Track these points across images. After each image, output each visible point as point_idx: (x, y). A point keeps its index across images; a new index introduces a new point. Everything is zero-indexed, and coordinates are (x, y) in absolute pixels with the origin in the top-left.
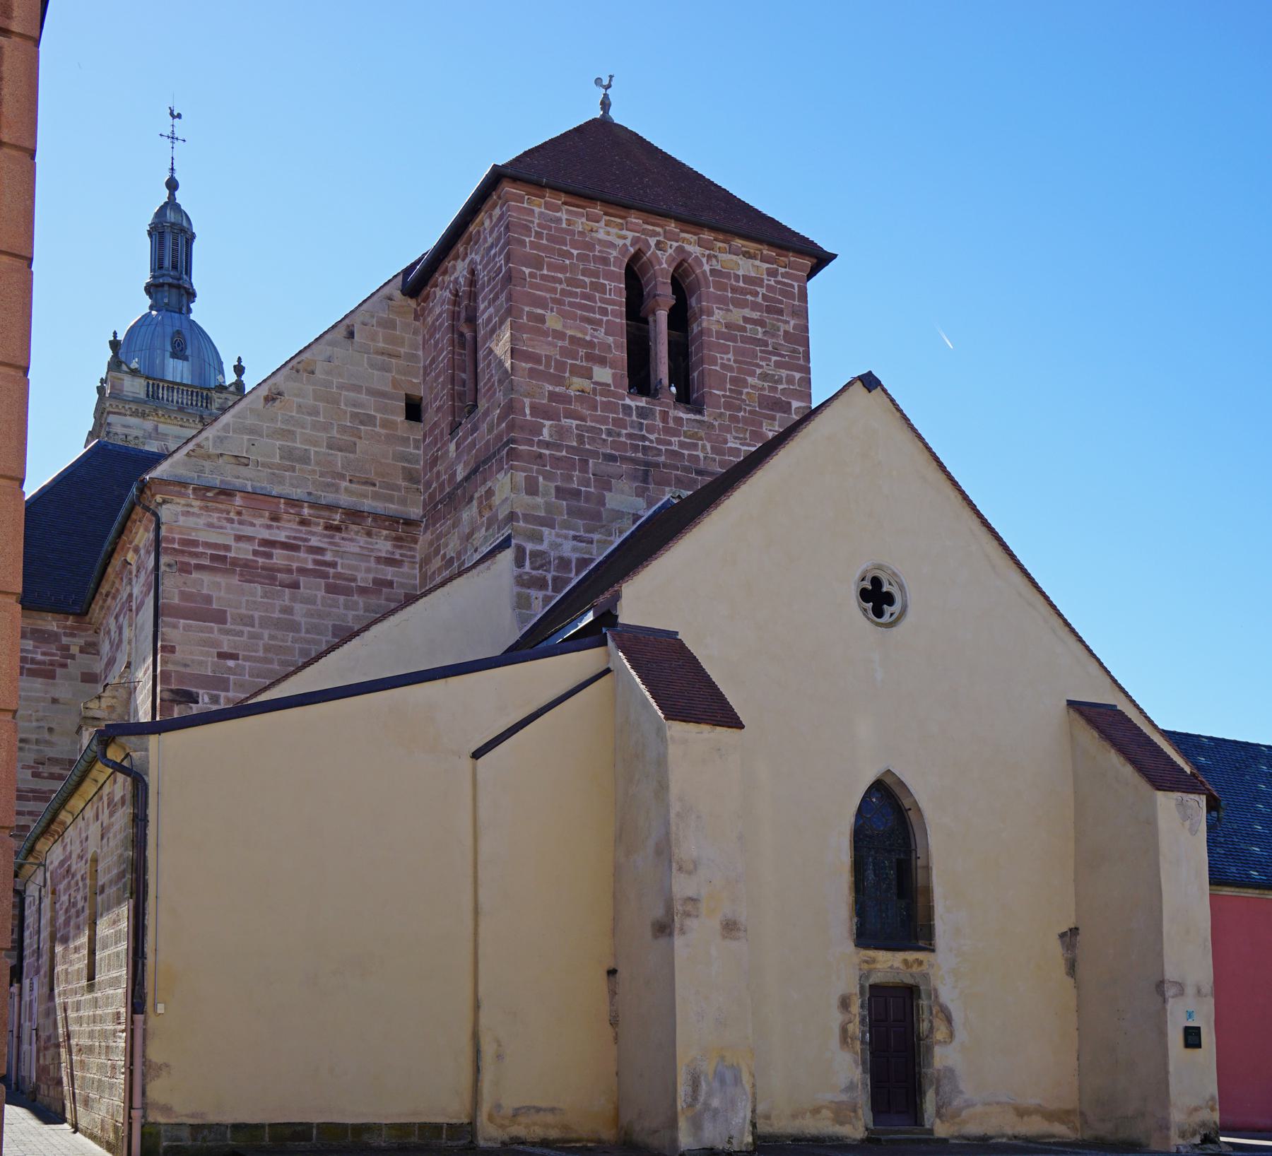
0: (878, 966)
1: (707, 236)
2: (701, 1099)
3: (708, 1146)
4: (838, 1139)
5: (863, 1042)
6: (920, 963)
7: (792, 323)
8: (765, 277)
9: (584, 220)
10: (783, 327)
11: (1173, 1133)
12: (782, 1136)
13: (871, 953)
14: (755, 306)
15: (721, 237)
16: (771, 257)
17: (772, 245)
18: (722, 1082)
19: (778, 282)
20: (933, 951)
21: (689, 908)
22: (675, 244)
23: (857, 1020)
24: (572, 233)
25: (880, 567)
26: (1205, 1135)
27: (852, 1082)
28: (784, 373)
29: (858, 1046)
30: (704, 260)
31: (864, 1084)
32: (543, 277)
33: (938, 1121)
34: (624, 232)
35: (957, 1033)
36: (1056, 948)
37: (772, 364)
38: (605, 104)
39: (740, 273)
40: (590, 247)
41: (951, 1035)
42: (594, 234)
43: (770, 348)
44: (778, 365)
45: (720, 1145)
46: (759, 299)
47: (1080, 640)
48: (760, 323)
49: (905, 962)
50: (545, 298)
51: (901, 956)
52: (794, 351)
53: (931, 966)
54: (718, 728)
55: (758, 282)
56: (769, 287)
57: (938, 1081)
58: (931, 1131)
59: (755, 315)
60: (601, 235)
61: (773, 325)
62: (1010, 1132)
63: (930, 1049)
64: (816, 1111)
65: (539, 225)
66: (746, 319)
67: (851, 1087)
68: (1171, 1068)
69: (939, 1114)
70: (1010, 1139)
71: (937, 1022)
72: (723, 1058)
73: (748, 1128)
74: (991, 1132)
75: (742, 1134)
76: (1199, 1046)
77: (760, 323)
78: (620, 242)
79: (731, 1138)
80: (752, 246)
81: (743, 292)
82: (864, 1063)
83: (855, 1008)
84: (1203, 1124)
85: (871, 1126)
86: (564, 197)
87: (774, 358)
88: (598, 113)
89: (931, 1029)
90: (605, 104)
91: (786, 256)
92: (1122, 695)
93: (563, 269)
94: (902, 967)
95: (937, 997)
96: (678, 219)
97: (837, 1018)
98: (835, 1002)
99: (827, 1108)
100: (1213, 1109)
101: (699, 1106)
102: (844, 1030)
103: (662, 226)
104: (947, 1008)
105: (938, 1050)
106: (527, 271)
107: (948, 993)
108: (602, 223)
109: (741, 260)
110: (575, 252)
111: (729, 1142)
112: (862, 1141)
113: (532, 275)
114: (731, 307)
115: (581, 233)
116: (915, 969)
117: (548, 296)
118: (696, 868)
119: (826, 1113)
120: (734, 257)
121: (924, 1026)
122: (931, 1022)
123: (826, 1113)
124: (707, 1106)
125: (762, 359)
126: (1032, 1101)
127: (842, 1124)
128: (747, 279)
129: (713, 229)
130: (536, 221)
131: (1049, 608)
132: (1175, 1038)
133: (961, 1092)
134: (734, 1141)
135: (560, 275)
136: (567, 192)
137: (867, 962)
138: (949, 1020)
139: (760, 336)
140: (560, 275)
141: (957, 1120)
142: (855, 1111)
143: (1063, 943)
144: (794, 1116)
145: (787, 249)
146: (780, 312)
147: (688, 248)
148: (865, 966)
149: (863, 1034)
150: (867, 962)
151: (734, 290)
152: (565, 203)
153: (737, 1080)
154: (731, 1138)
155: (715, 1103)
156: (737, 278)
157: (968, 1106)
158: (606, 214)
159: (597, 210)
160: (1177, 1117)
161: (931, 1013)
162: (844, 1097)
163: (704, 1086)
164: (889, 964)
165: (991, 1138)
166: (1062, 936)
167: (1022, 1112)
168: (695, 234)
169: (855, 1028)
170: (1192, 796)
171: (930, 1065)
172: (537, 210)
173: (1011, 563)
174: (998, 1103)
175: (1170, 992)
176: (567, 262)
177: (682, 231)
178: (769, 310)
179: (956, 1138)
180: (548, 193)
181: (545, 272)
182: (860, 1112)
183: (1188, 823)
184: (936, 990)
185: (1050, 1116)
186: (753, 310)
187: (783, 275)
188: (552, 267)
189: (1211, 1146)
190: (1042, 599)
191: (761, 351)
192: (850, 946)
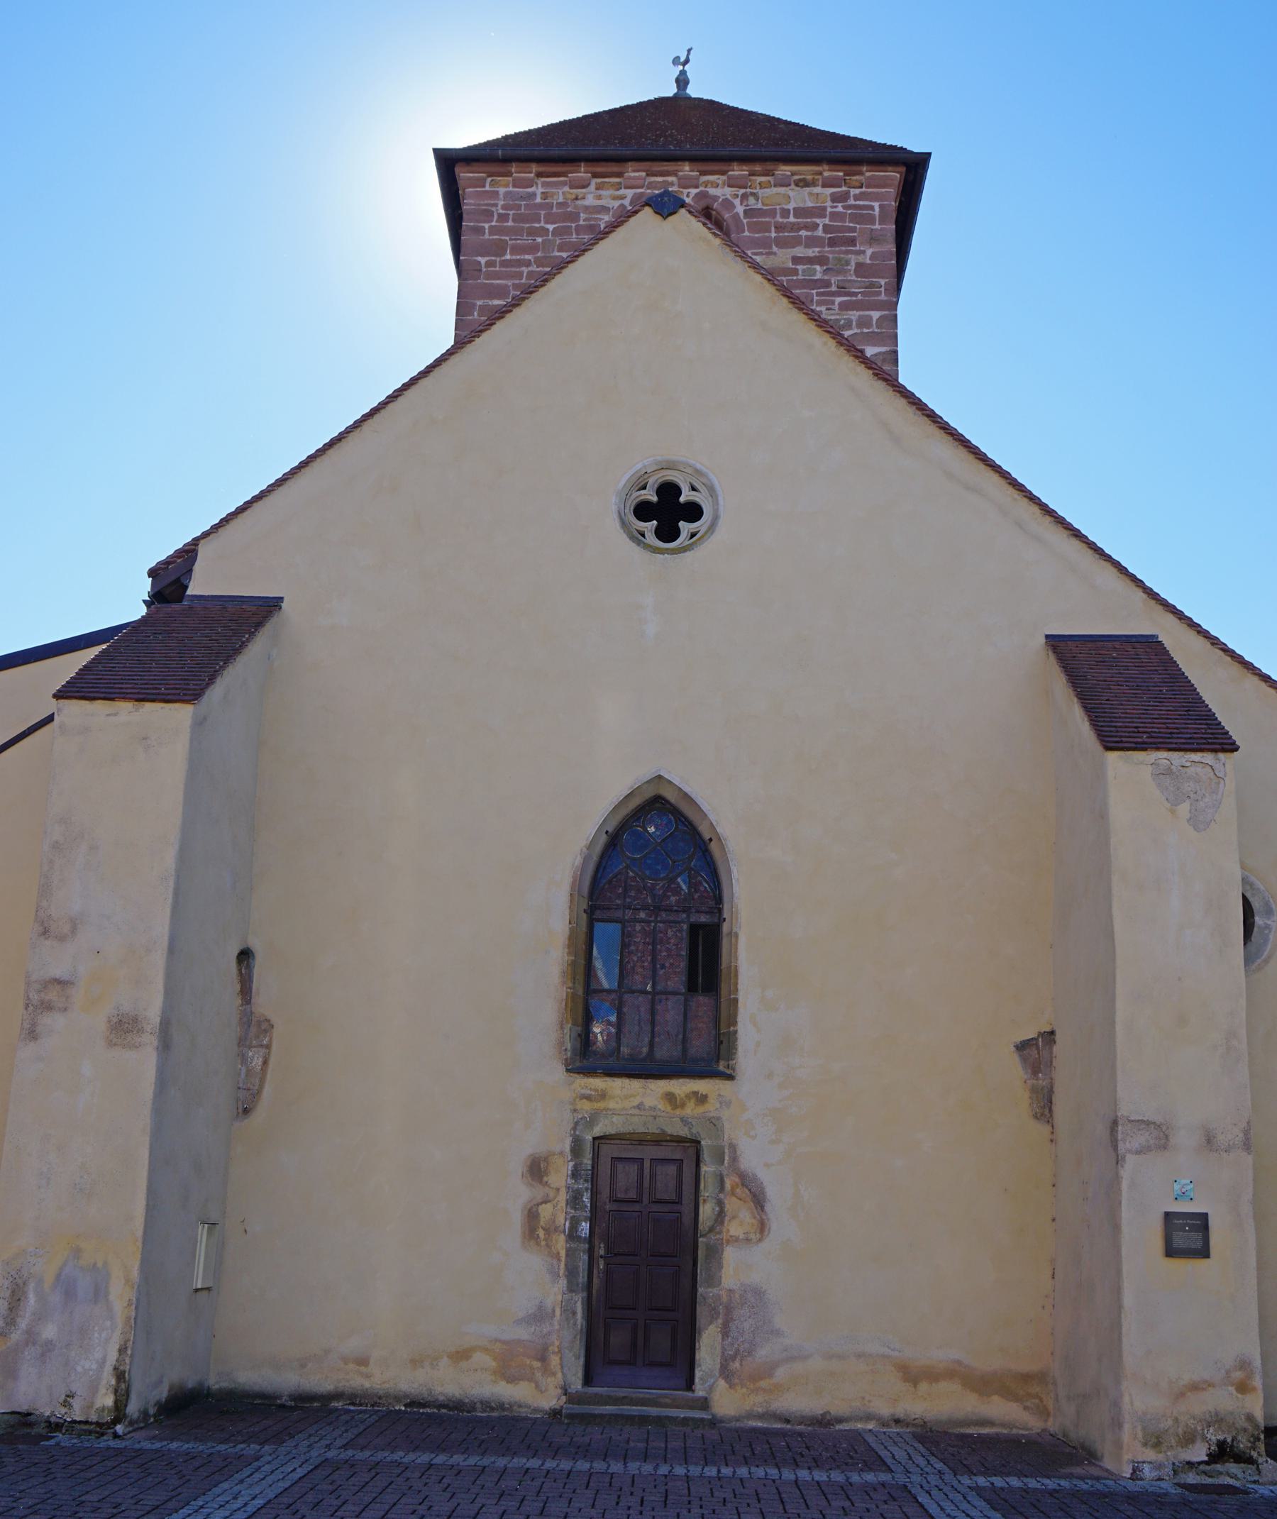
0: (612, 1104)
1: (738, 171)
2: (23, 1324)
3: (24, 1408)
4: (501, 1406)
5: (572, 1236)
6: (702, 1099)
7: (869, 252)
8: (829, 204)
9: (566, 189)
10: (853, 259)
11: (1130, 1435)
12: (387, 1395)
13: (598, 1083)
14: (811, 242)
15: (758, 168)
16: (837, 178)
17: (834, 162)
18: (69, 1293)
19: (850, 207)
20: (730, 1077)
21: (52, 995)
22: (694, 191)
23: (563, 1197)
24: (551, 206)
25: (671, 466)
26: (1221, 1444)
27: (540, 1307)
28: (854, 315)
29: (560, 1243)
30: (737, 202)
31: (569, 1312)
32: (505, 263)
33: (722, 1383)
34: (622, 192)
35: (774, 1226)
36: (1015, 1070)
37: (836, 307)
38: (682, 81)
39: (791, 206)
40: (574, 217)
41: (762, 1227)
42: (579, 202)
43: (834, 288)
44: (844, 307)
45: (47, 1408)
46: (820, 232)
47: (1077, 534)
48: (821, 260)
49: (670, 1097)
50: (506, 286)
51: (660, 1087)
52: (872, 285)
53: (726, 1104)
54: (148, 705)
55: (820, 212)
56: (834, 216)
57: (729, 1310)
58: (704, 1404)
59: (811, 252)
60: (590, 201)
61: (840, 260)
62: (885, 1411)
63: (715, 1253)
64: (461, 1355)
65: (504, 207)
66: (796, 260)
67: (539, 1316)
68: (1128, 1300)
69: (725, 1372)
70: (884, 1424)
71: (731, 1204)
72: (77, 1252)
73: (108, 1379)
74: (837, 1407)
75: (94, 1390)
76: (1203, 1252)
77: (821, 260)
78: (616, 204)
79: (70, 1395)
80: (806, 171)
81: (795, 228)
82: (571, 1273)
83: (560, 1177)
84: (1217, 1420)
85: (577, 1384)
86: (535, 168)
87: (838, 300)
88: (670, 90)
89: (720, 1216)
90: (682, 81)
91: (861, 173)
92: (1171, 618)
93: (533, 249)
94: (662, 1106)
95: (734, 1159)
96: (693, 159)
97: (520, 1193)
98: (517, 1165)
99: (485, 1350)
100: (1243, 1388)
101: (15, 1336)
102: (532, 1216)
103: (674, 174)
104: (755, 1178)
105: (730, 1255)
106: (483, 260)
107: (757, 1151)
108: (592, 187)
109: (793, 192)
110: (551, 227)
111: (66, 1404)
112: (555, 1413)
113: (489, 264)
114: (775, 249)
115: (560, 205)
116: (690, 1110)
117: (510, 283)
118: (74, 930)
119: (482, 1359)
120: (782, 190)
121: (707, 1211)
122: (720, 1203)
123: (482, 1359)
124: (31, 1337)
125: (820, 303)
126: (939, 1355)
127: (512, 1380)
128: (799, 212)
129: (744, 160)
130: (501, 203)
131: (1011, 490)
132: (1141, 1236)
133: (778, 1333)
134: (77, 1404)
135: (527, 257)
136: (539, 160)
137: (588, 1098)
138: (758, 1200)
139: (818, 276)
140: (527, 257)
141: (763, 1384)
142: (543, 1358)
143: (1024, 1060)
144: (416, 1362)
145: (859, 162)
146: (852, 242)
147: (712, 191)
148: (586, 1106)
149: (575, 1223)
150: (588, 1098)
151: (779, 228)
152: (539, 175)
153: (99, 1293)
154: (70, 1395)
155: (49, 1331)
156: (785, 213)
157: (792, 1359)
158: (595, 175)
159: (582, 173)
160: (1141, 1401)
161: (722, 1188)
162: (523, 1333)
163: (32, 1299)
164: (636, 1102)
165: (840, 1420)
166: (1022, 1047)
167: (912, 1376)
168: (723, 173)
169: (556, 1212)
170: (1196, 757)
171: (713, 1280)
172: (502, 190)
173: (932, 429)
174: (859, 1356)
175: (1130, 1141)
176: (539, 240)
177: (703, 173)
178: (832, 242)
179: (761, 1417)
180: (513, 168)
181: (508, 257)
182: (554, 1361)
183: (1184, 809)
184: (733, 1147)
185: (983, 1384)
186: (807, 246)
187: (857, 198)
188: (515, 250)
189: (1233, 1467)
190: (996, 477)
191: (818, 294)
192: (557, 1072)
